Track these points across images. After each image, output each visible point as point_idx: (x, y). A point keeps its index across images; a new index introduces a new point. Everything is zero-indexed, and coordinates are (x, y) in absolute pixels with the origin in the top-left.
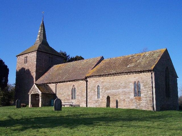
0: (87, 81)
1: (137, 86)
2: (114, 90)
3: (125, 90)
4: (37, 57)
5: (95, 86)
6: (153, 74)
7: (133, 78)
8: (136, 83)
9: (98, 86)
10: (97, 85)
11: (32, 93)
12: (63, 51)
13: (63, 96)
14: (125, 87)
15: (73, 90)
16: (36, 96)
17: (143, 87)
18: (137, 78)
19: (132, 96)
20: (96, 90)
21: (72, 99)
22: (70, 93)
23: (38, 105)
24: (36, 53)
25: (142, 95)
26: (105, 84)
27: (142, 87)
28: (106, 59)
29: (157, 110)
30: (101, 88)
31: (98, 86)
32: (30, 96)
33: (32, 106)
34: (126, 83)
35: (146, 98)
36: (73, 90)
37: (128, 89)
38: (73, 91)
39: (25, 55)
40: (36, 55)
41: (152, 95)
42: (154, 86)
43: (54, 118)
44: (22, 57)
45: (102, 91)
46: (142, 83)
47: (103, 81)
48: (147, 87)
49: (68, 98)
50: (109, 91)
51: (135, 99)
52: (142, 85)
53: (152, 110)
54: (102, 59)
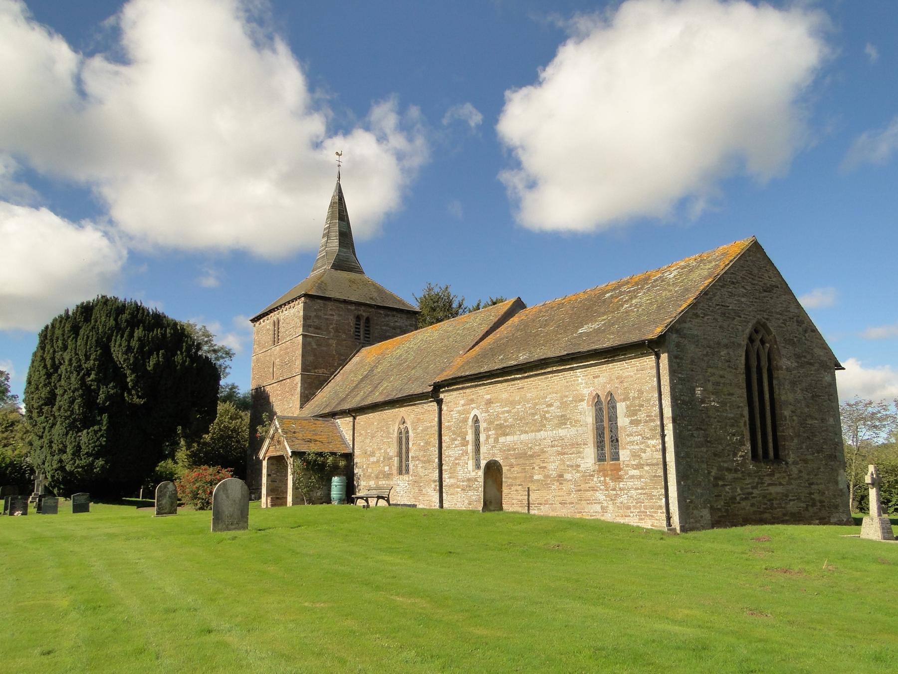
0: (440, 402)
1: (605, 411)
2: (526, 432)
3: (562, 432)
4: (306, 318)
5: (465, 420)
6: (664, 357)
7: (587, 381)
8: (603, 398)
9: (476, 420)
10: (472, 416)
11: (269, 454)
12: (161, 310)
13: (373, 463)
14: (563, 421)
15: (403, 436)
16: (278, 462)
17: (627, 420)
18: (602, 380)
19: (589, 454)
20: (470, 437)
21: (400, 473)
22: (393, 451)
23: (284, 503)
24: (301, 305)
25: (624, 454)
26: (496, 408)
27: (623, 421)
28: (533, 306)
29: (684, 529)
30: (483, 425)
31: (476, 420)
32: (265, 463)
33: (269, 504)
34: (564, 405)
35: (639, 466)
36: (403, 436)
37: (573, 431)
38: (403, 440)
39: (273, 316)
40: (301, 313)
41: (659, 455)
42: (668, 412)
43: (518, 516)
44: (267, 323)
45: (488, 437)
46: (624, 400)
47: (488, 397)
48: (642, 416)
49: (387, 468)
50: (509, 438)
51: (599, 471)
52: (621, 407)
53: (666, 529)
54: (519, 305)
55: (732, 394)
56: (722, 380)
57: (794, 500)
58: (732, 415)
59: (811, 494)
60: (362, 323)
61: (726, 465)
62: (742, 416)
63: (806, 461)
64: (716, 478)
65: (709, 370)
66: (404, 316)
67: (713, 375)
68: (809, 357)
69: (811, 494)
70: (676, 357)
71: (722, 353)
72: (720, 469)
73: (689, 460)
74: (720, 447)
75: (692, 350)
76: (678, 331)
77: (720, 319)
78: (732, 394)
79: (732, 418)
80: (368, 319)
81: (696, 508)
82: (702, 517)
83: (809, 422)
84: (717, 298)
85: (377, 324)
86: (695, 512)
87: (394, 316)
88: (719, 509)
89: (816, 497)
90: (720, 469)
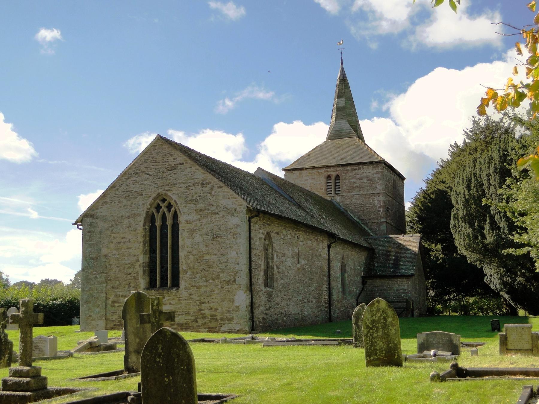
55: (131, 248)
56: (123, 240)
57: (182, 315)
58: (129, 262)
59: (201, 310)
60: (332, 181)
61: (121, 294)
62: (137, 261)
63: (198, 287)
64: (113, 302)
65: (113, 235)
66: (370, 167)
67: (114, 238)
68: (212, 209)
69: (201, 310)
70: (89, 232)
71: (125, 223)
72: (116, 296)
73: (91, 292)
74: (118, 283)
75: (101, 225)
76: (92, 216)
77: (124, 200)
78: (131, 248)
79: (129, 264)
80: (338, 177)
81: (94, 319)
82: (98, 325)
83: (207, 257)
84: (123, 187)
85: (345, 179)
86: (93, 322)
87: (360, 169)
88: (113, 321)
89: (207, 312)
90: (116, 296)
